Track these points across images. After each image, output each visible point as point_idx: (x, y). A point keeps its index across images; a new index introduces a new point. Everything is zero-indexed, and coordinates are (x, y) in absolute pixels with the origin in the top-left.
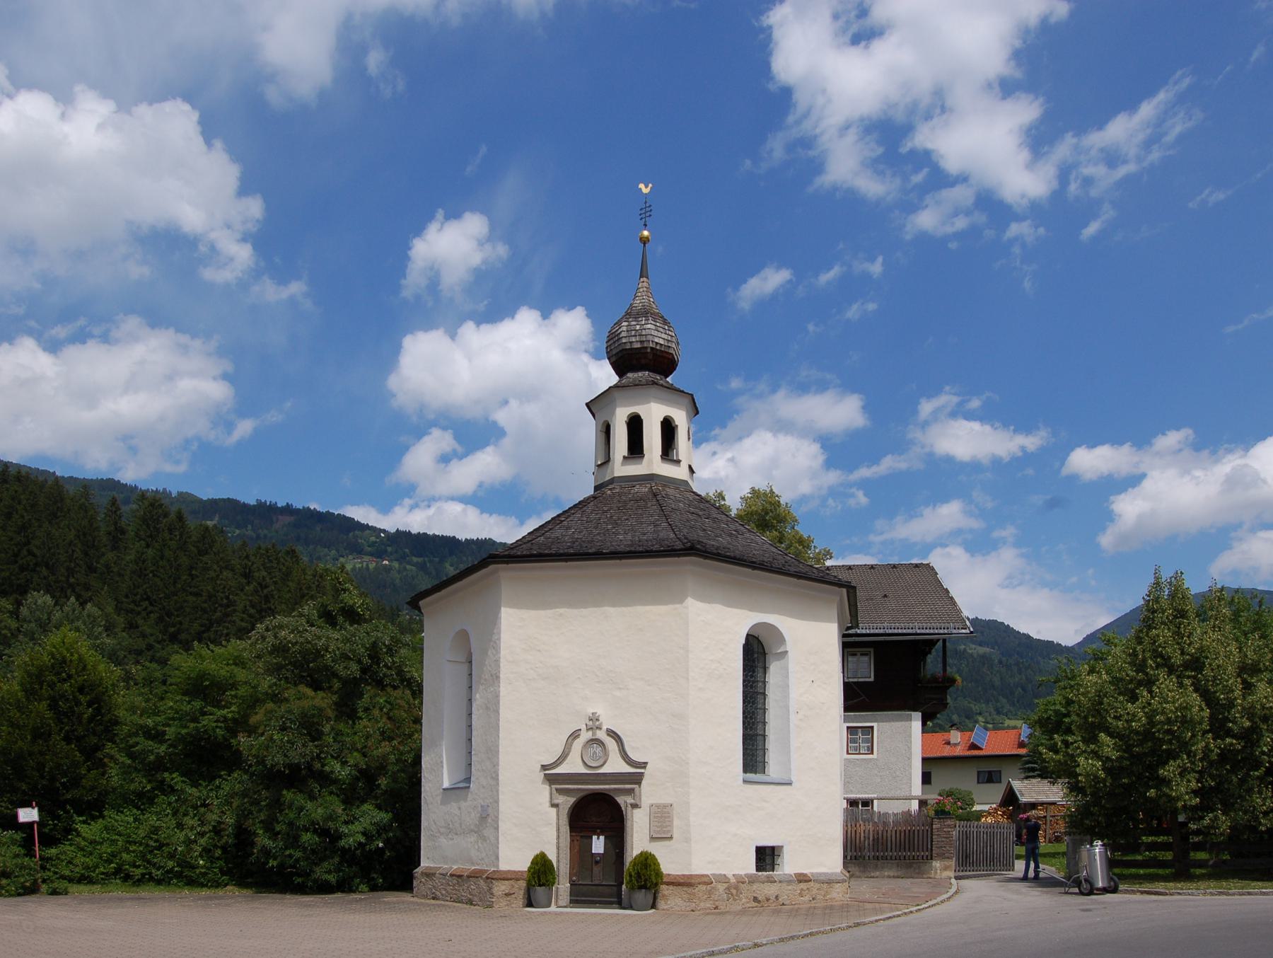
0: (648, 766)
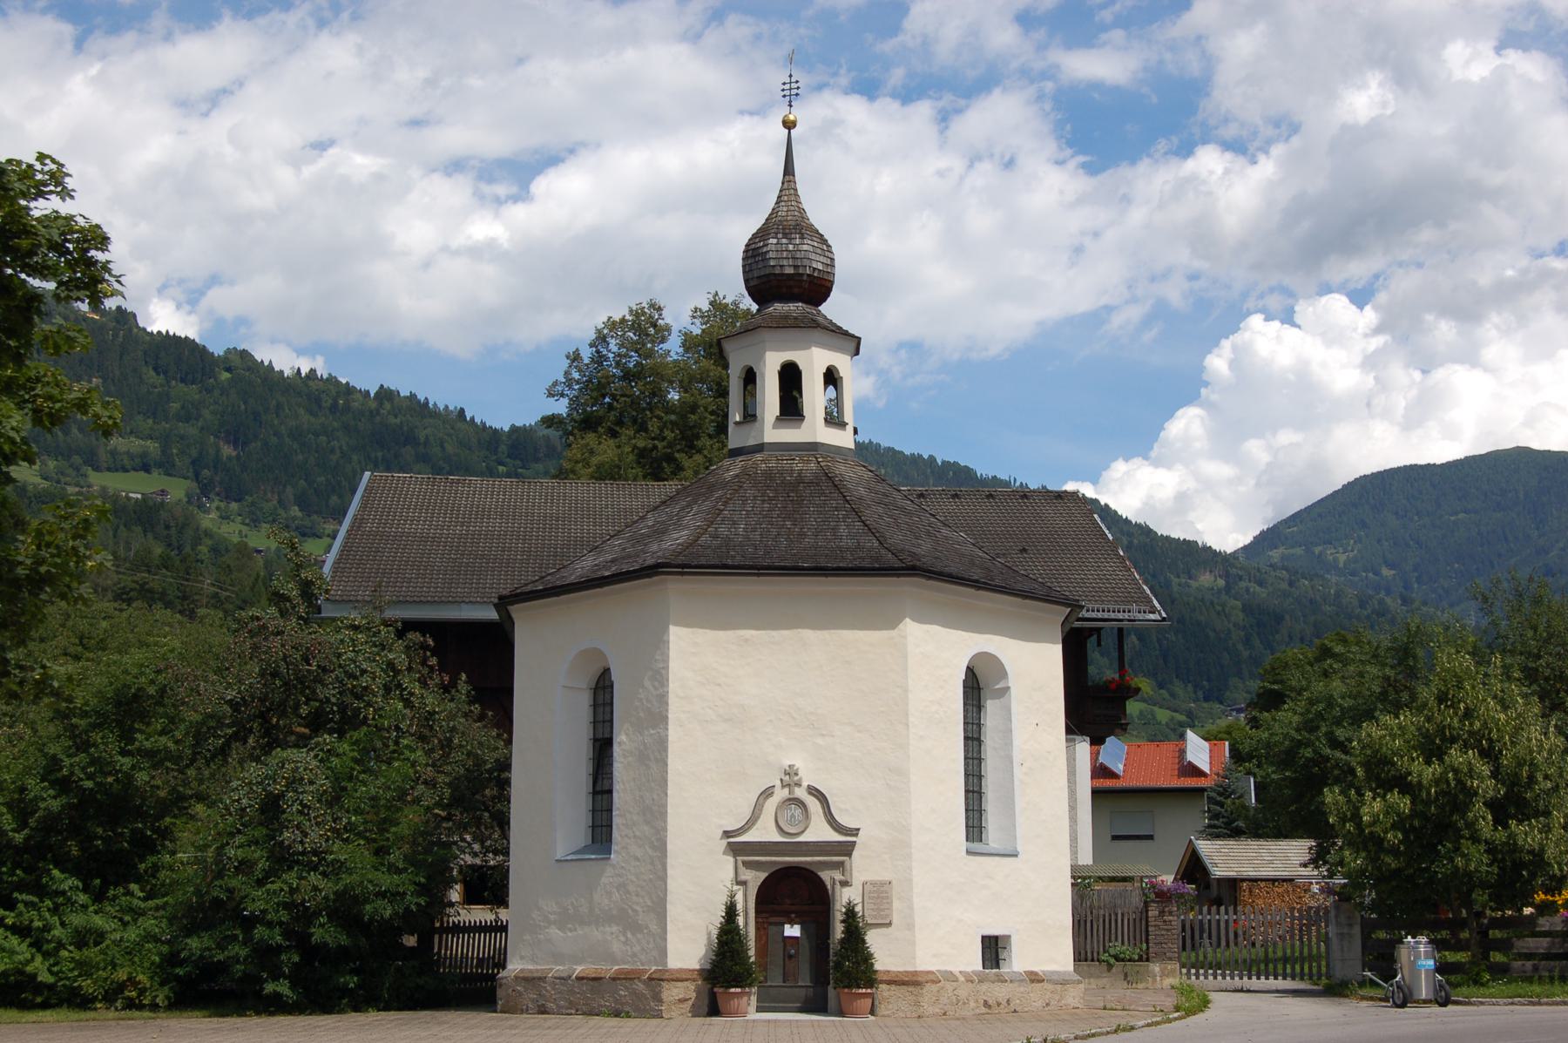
0: (861, 832)
